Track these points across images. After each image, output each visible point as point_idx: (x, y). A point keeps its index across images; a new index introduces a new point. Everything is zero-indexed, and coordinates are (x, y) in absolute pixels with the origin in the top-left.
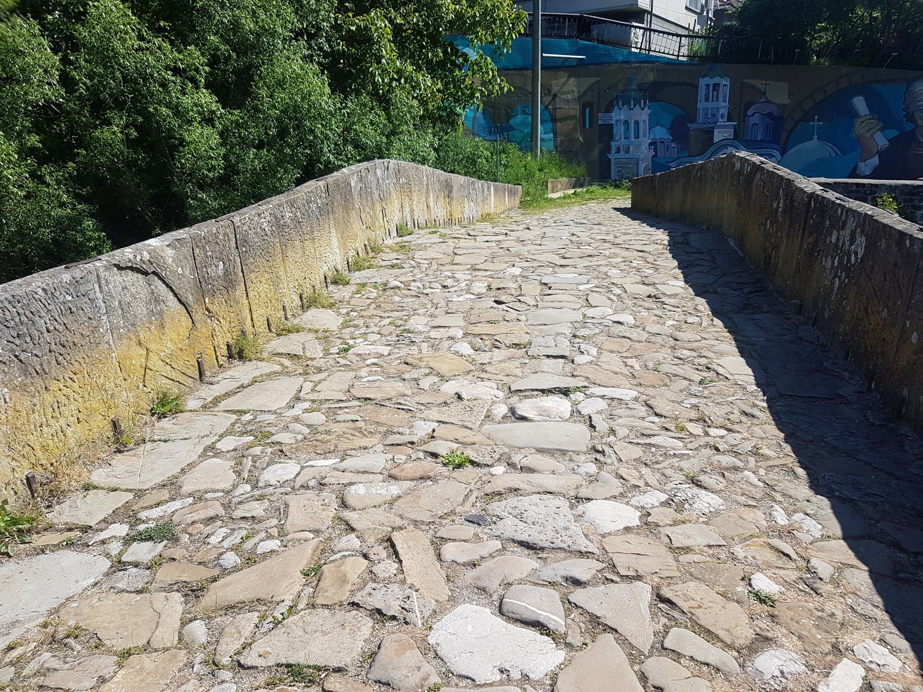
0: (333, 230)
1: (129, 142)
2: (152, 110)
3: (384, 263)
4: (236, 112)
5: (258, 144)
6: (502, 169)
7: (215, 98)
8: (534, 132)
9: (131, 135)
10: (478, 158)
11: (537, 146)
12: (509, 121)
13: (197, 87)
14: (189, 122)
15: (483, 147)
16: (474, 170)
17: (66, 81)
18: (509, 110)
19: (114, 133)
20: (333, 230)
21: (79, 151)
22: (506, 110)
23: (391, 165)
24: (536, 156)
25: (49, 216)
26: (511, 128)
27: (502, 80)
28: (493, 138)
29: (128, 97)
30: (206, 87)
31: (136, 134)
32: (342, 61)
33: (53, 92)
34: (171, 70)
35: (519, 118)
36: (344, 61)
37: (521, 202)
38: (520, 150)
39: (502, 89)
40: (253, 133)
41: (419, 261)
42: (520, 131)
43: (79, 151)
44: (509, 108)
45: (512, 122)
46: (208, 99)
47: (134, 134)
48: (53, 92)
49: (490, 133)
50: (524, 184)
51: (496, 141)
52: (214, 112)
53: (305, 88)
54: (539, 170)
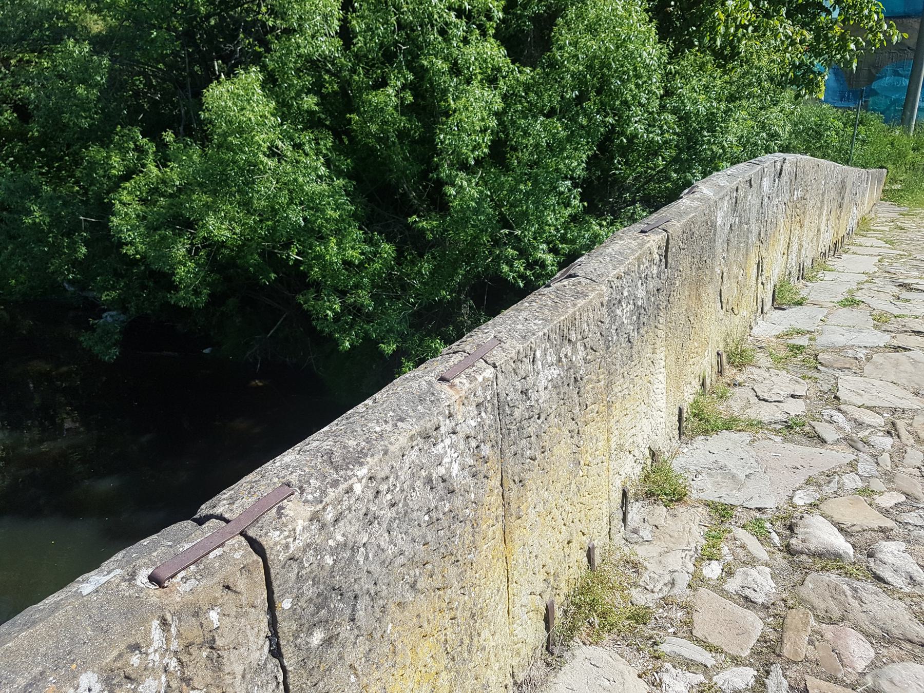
0: (661, 353)
1: (403, 109)
2: (425, 63)
3: (766, 413)
4: (527, 70)
5: (549, 112)
6: (857, 145)
7: (504, 51)
8: (911, 99)
9: (406, 99)
10: (826, 130)
11: (911, 118)
12: (871, 84)
13: (484, 34)
14: (468, 82)
15: (834, 118)
16: (818, 145)
17: (346, 34)
18: (873, 71)
19: (389, 96)
20: (661, 353)
21: (352, 116)
22: (869, 70)
23: (787, 167)
24: (909, 130)
25: (303, 190)
26: (874, 93)
27: (890, 26)
28: (845, 104)
29: (400, 48)
30: (495, 36)
31: (411, 98)
32: (673, 3)
33: (328, 46)
34: (454, 10)
35: (887, 80)
36: (676, 4)
37: (883, 191)
38: (886, 122)
39: (889, 38)
40: (551, 98)
41: (857, 413)
42: (886, 97)
43: (352, 116)
44: (875, 67)
45: (875, 86)
46: (495, 51)
47: (410, 99)
48: (328, 46)
49: (842, 98)
50: (890, 166)
51: (850, 108)
52: (499, 70)
53: (623, 32)
54: (913, 149)
